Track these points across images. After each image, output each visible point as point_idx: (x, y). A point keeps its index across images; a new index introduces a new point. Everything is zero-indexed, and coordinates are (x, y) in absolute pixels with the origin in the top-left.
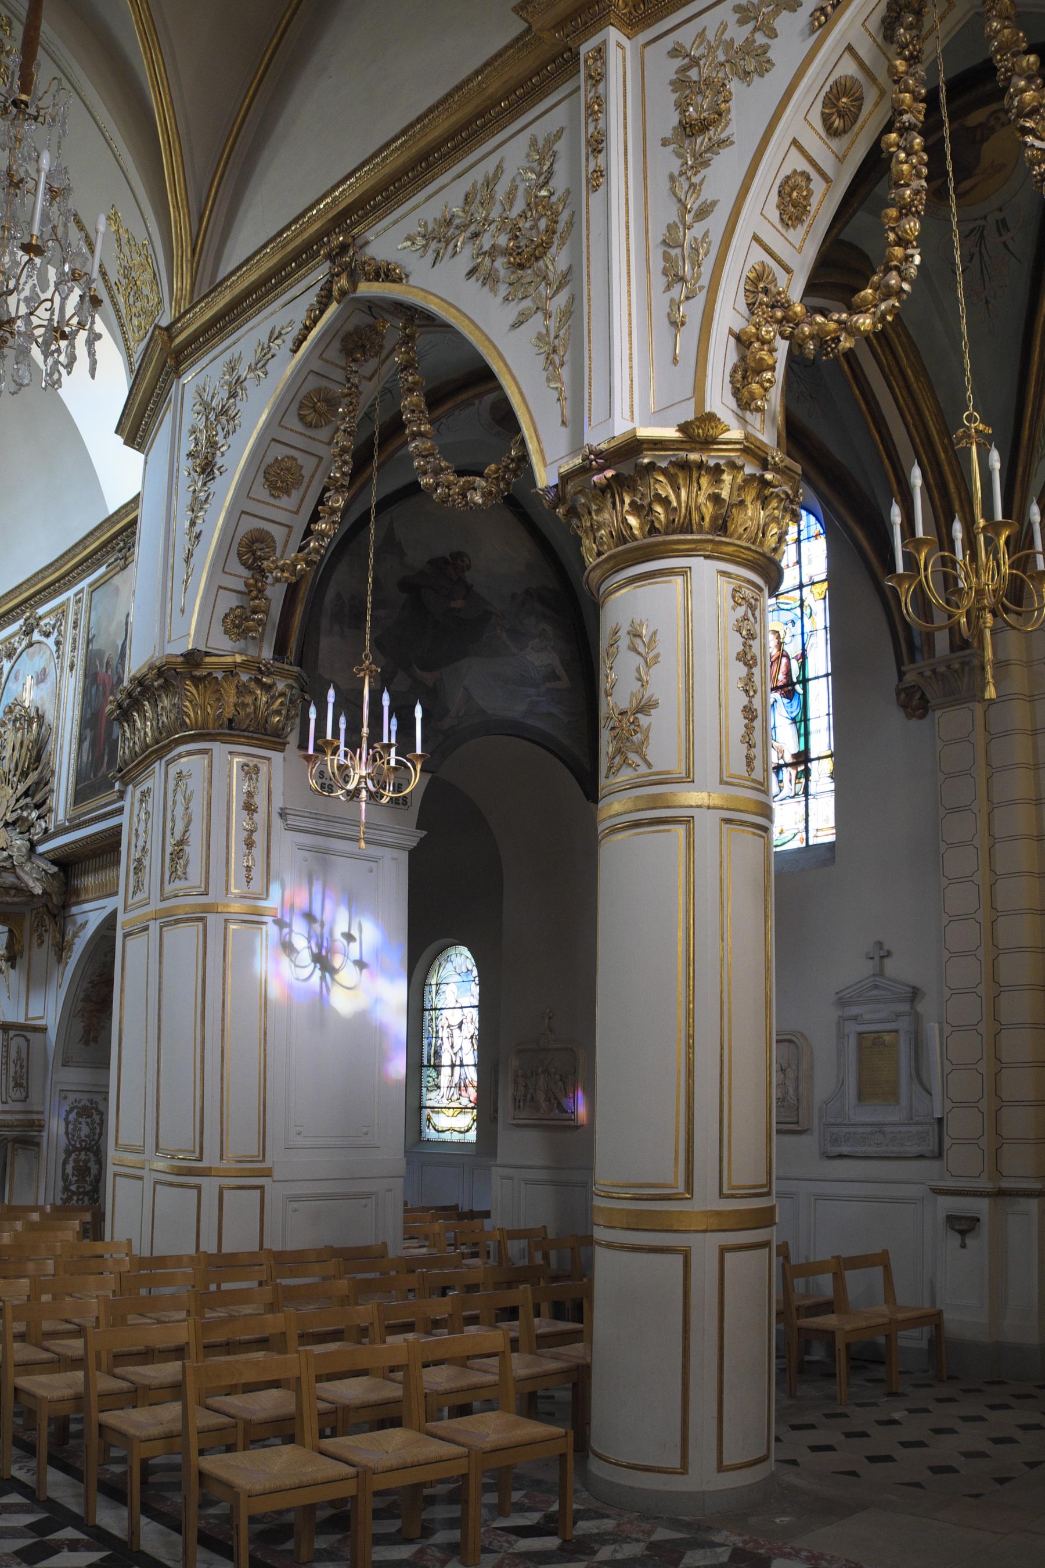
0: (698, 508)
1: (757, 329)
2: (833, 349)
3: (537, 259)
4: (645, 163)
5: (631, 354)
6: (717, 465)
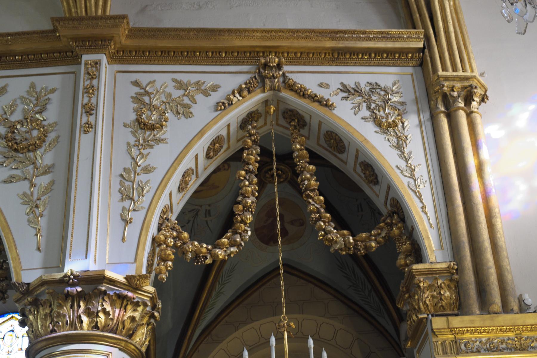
0: (123, 322)
1: (166, 238)
2: (202, 261)
3: (29, 151)
4: (113, 131)
5: (97, 228)
6: (138, 302)
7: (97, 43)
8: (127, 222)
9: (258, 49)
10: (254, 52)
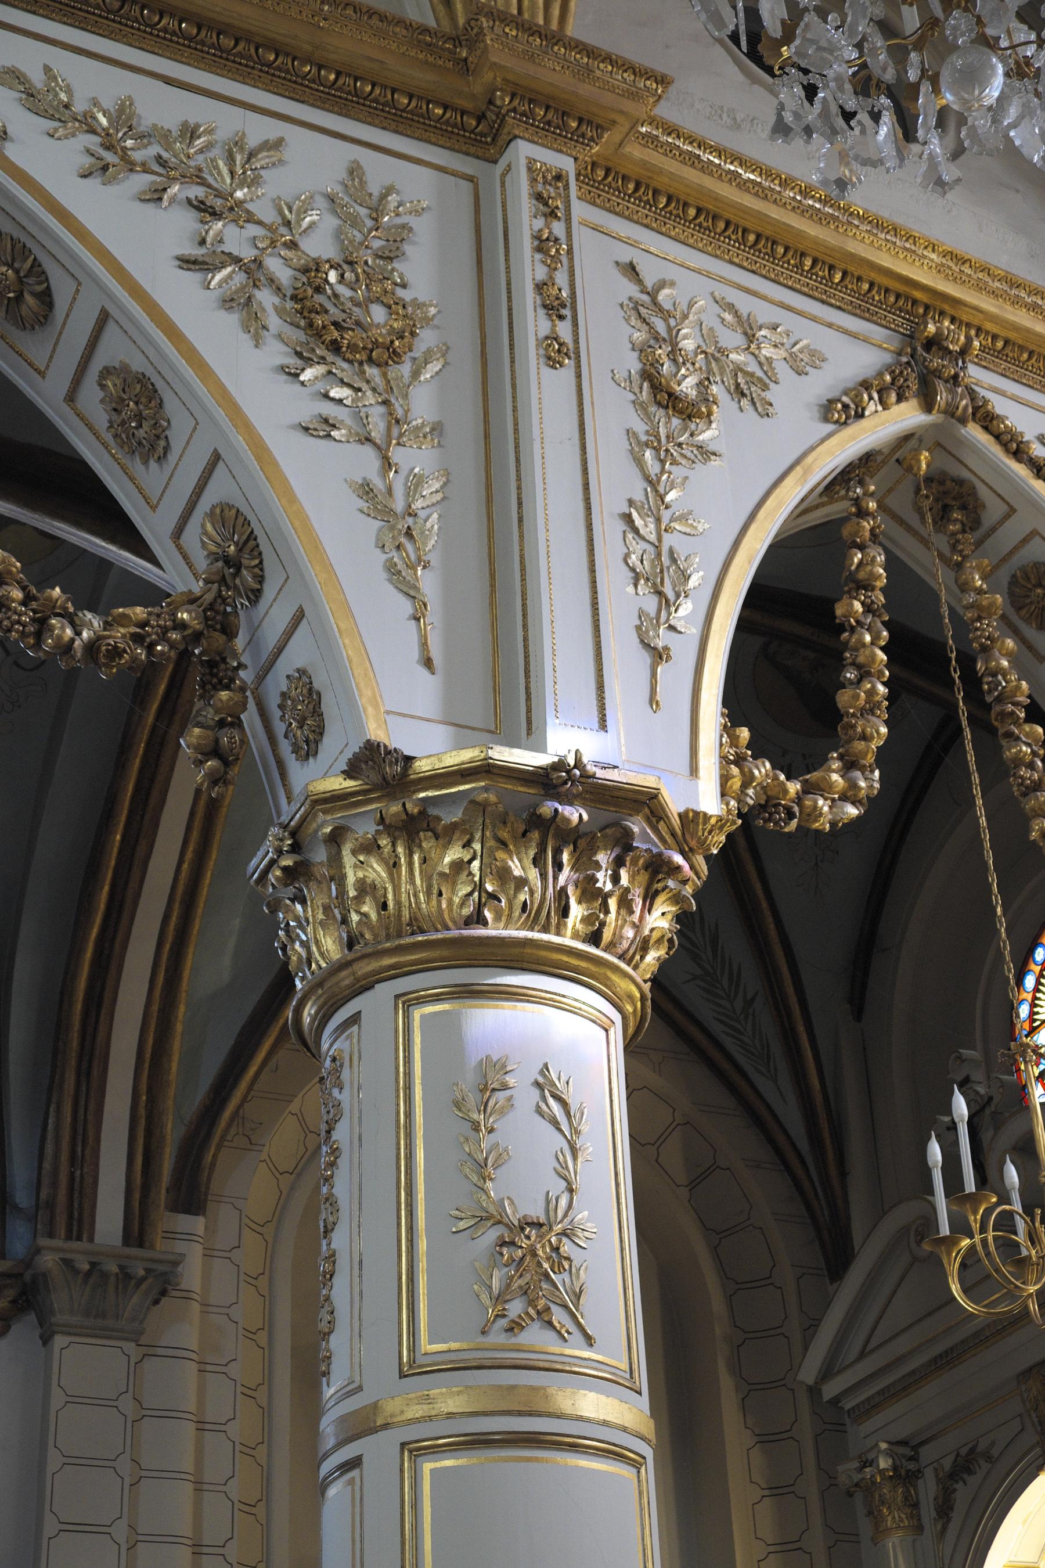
7: (564, 119)
8: (659, 655)
9: (918, 295)
10: (907, 298)
